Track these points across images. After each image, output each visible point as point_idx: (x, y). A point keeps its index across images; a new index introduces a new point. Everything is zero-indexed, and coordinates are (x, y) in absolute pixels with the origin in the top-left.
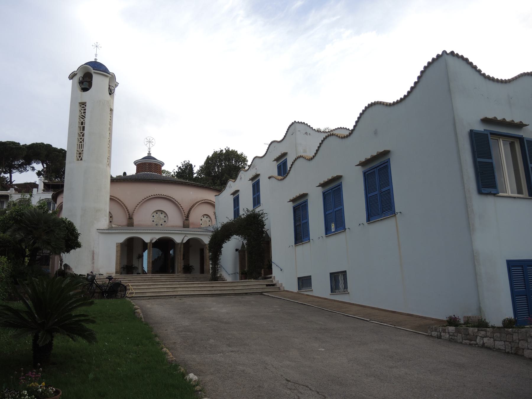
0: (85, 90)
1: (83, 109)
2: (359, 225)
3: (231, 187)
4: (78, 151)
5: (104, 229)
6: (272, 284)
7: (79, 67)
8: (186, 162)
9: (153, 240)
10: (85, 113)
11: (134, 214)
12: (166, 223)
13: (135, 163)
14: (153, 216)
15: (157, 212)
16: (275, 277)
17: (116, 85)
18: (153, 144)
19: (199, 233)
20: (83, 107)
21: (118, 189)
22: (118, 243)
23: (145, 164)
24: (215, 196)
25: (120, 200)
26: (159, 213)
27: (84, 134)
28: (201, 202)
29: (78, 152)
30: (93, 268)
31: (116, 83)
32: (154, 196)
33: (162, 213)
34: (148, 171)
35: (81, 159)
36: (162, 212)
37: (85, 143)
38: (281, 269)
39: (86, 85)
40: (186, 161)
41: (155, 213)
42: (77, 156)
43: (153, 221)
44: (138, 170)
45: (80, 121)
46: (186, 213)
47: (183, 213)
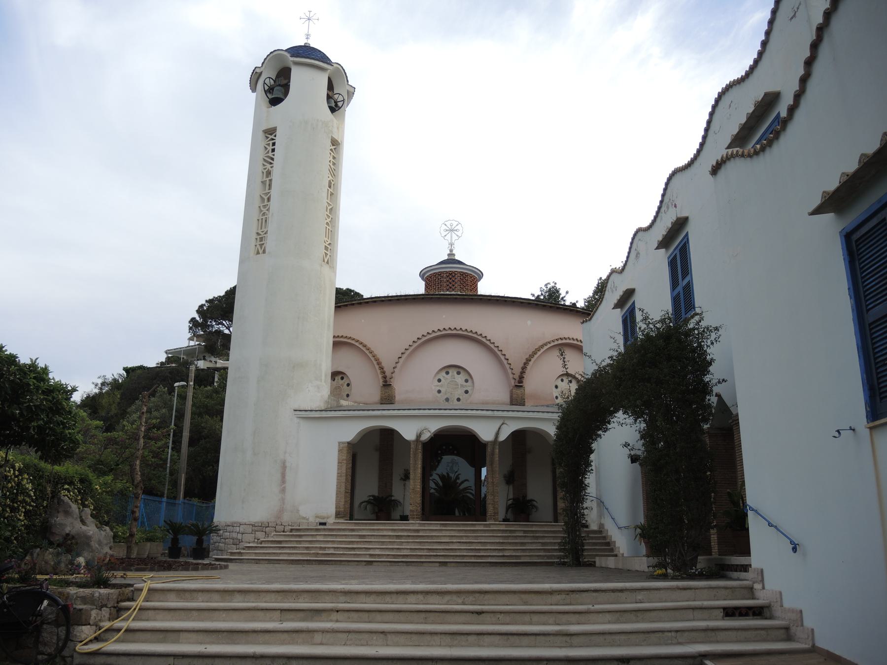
0: (275, 102)
1: (271, 142)
2: (837, 434)
3: (614, 289)
4: (258, 234)
5: (314, 408)
6: (749, 608)
7: (265, 59)
8: (549, 286)
9: (422, 436)
10: (273, 150)
11: (393, 375)
12: (470, 396)
13: (422, 275)
14: (439, 380)
15: (447, 369)
16: (762, 571)
17: (348, 92)
18: (459, 233)
19: (540, 415)
20: (273, 139)
21: (363, 321)
22: (343, 443)
23: (440, 274)
24: (583, 322)
25: (365, 346)
26: (453, 372)
27: (270, 196)
28: (552, 344)
29: (258, 237)
30: (284, 503)
31: (348, 88)
32: (439, 333)
33: (459, 373)
34: (448, 290)
35: (264, 252)
36: (459, 369)
37: (273, 214)
38: (792, 542)
39: (277, 94)
40: (549, 283)
41: (444, 374)
42: (256, 246)
43: (439, 392)
44: (427, 287)
45: (265, 169)
46: (517, 371)
47: (509, 371)
